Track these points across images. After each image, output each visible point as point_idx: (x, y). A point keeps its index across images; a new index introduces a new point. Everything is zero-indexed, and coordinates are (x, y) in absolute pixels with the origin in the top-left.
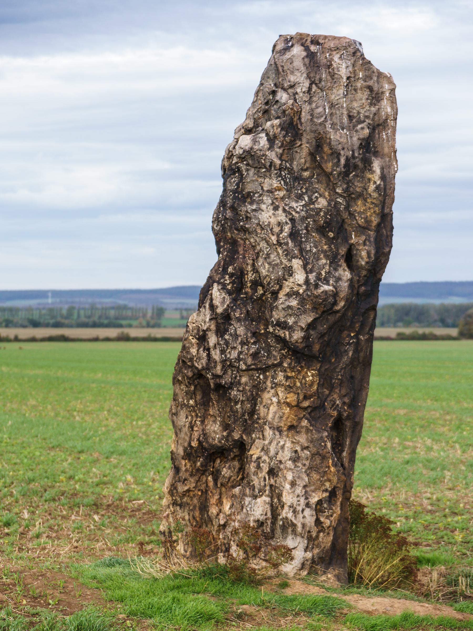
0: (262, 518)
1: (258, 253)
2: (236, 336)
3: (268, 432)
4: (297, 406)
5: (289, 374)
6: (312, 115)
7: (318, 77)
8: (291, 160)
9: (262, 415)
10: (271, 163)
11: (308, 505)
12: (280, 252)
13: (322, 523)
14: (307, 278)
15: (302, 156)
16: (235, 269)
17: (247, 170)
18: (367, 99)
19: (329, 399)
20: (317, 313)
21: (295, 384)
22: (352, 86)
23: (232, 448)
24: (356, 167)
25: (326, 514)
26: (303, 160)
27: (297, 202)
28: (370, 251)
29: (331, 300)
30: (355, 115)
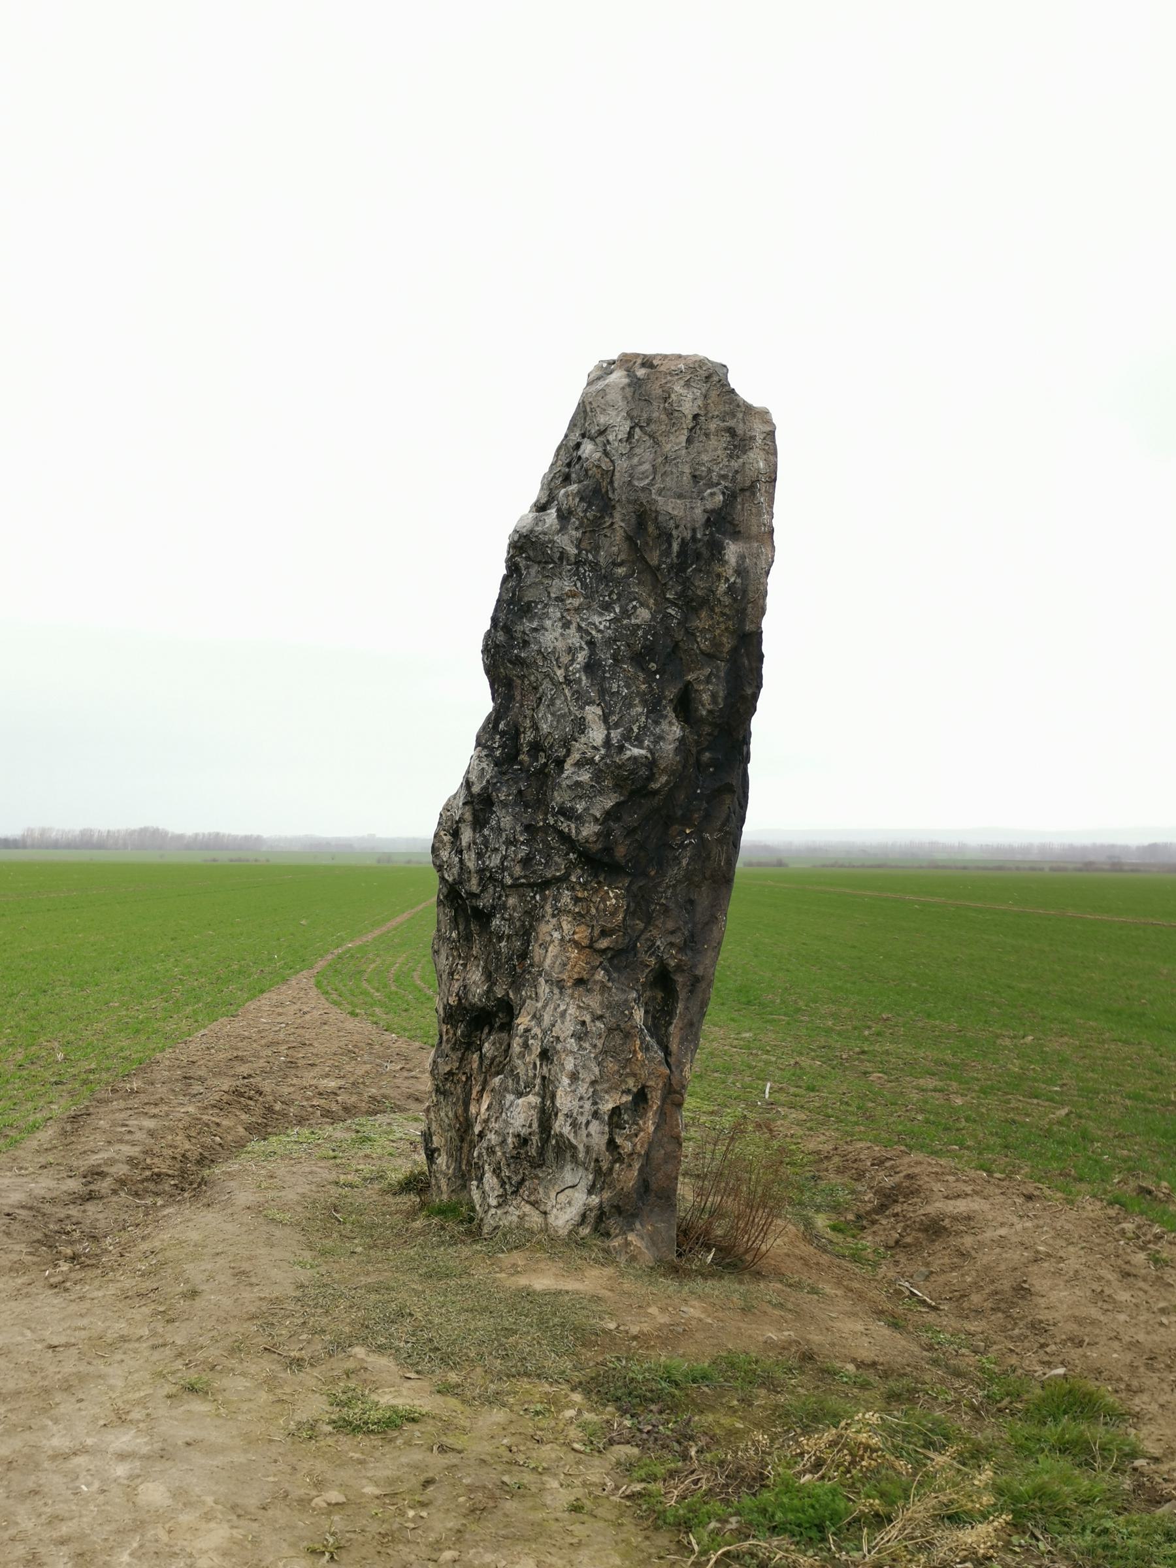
0: (524, 1132)
1: (540, 699)
2: (499, 830)
3: (544, 988)
4: (590, 947)
5: (580, 895)
6: (631, 475)
7: (645, 416)
8: (597, 548)
9: (536, 959)
10: (562, 553)
11: (596, 1115)
12: (568, 694)
13: (618, 1147)
14: (608, 736)
15: (614, 544)
16: (507, 725)
17: (527, 567)
18: (725, 449)
19: (643, 937)
20: (621, 794)
21: (588, 911)
22: (701, 429)
23: (497, 1012)
24: (698, 556)
25: (627, 1131)
26: (615, 549)
27: (601, 614)
28: (717, 692)
29: (644, 772)
30: (704, 474)
